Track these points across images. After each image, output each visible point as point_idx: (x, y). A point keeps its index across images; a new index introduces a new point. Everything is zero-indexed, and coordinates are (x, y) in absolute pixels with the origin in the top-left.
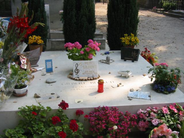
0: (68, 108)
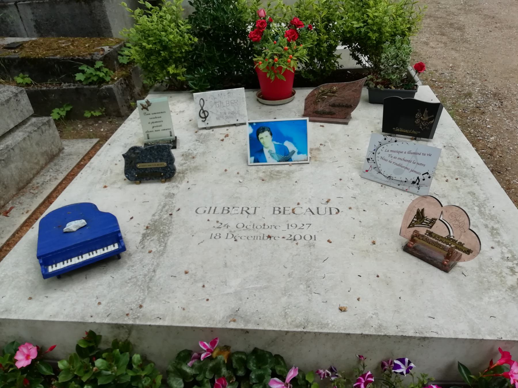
0: (112, 37)
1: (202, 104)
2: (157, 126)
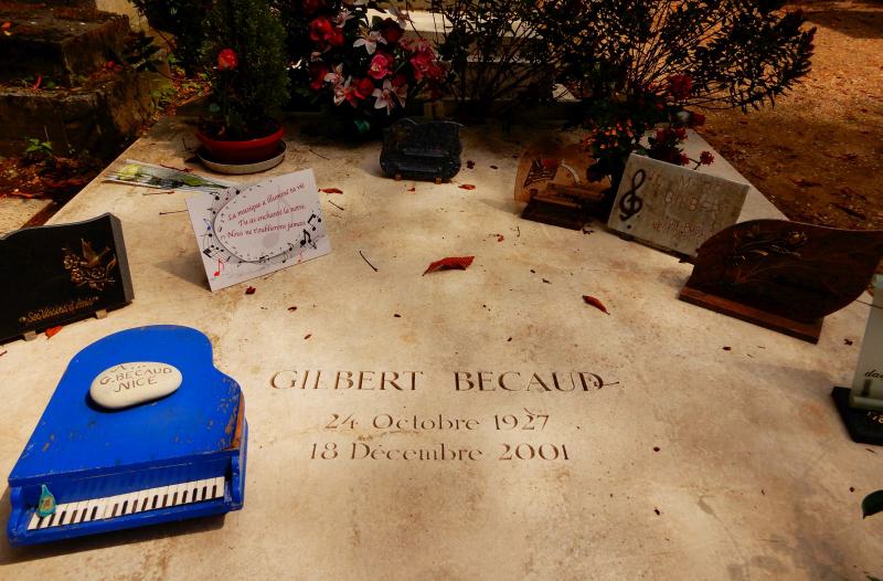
1: (637, 182)
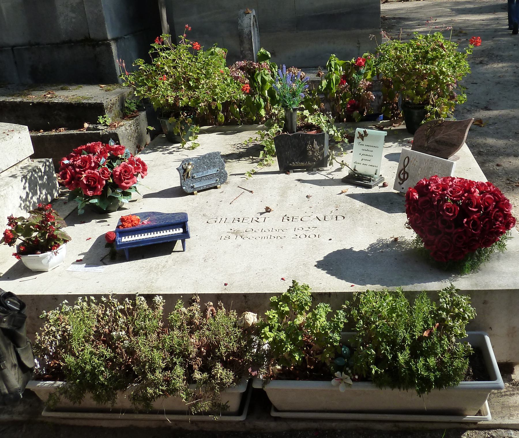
1: (406, 163)
2: (366, 160)
